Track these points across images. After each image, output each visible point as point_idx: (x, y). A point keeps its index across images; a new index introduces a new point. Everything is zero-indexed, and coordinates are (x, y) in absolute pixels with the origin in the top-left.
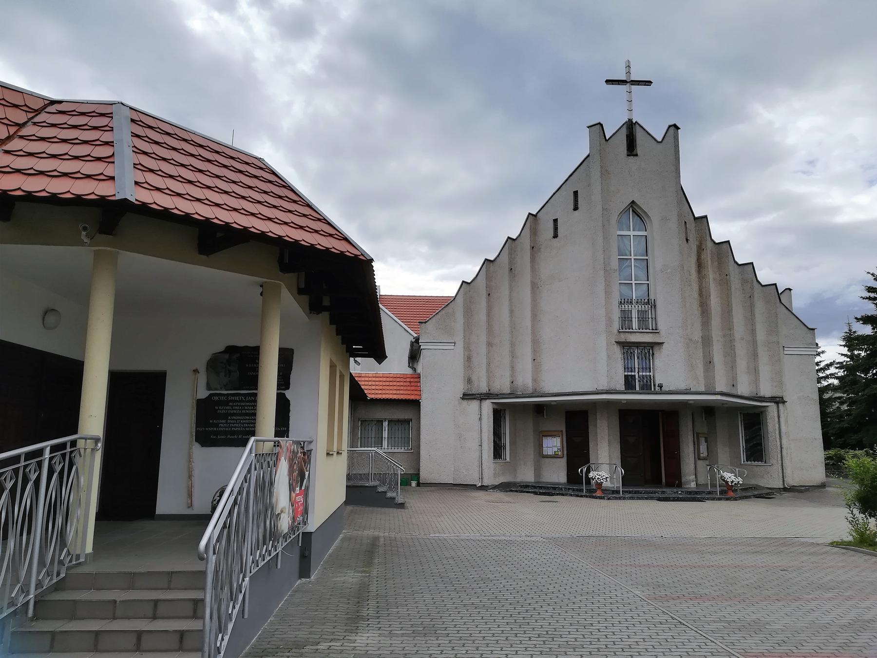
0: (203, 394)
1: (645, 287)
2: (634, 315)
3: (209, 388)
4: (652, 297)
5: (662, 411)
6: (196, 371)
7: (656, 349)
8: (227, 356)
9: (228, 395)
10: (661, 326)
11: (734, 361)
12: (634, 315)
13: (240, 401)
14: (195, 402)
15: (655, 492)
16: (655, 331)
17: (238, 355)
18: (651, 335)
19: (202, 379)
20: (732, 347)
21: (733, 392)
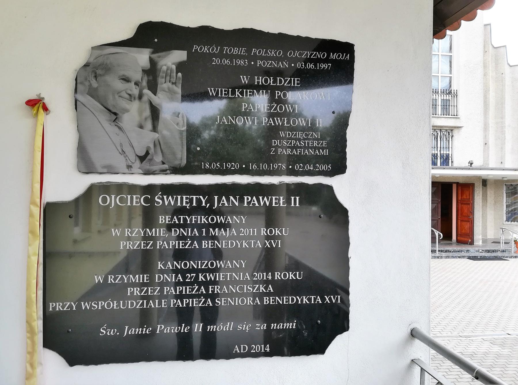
0: (67, 184)
1: (448, 79)
2: (439, 103)
3: (85, 163)
4: (454, 88)
5: (458, 184)
6: (36, 104)
7: (455, 132)
8: (142, 57)
9: (150, 189)
10: (461, 113)
11: (503, 143)
12: (439, 103)
13: (191, 211)
14: (37, 212)
15: (461, 251)
16: (456, 116)
17: (179, 56)
18: (453, 120)
19: (61, 128)
20: (503, 133)
21: (502, 166)
